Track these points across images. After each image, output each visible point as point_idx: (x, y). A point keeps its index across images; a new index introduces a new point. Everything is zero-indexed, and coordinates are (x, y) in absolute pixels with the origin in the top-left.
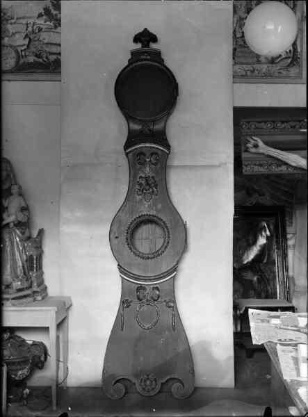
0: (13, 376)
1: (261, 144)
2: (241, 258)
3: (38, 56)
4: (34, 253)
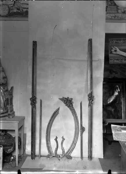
0: (6, 152)
1: (118, 50)
2: (107, 101)
3: (18, 9)
4: (9, 97)
